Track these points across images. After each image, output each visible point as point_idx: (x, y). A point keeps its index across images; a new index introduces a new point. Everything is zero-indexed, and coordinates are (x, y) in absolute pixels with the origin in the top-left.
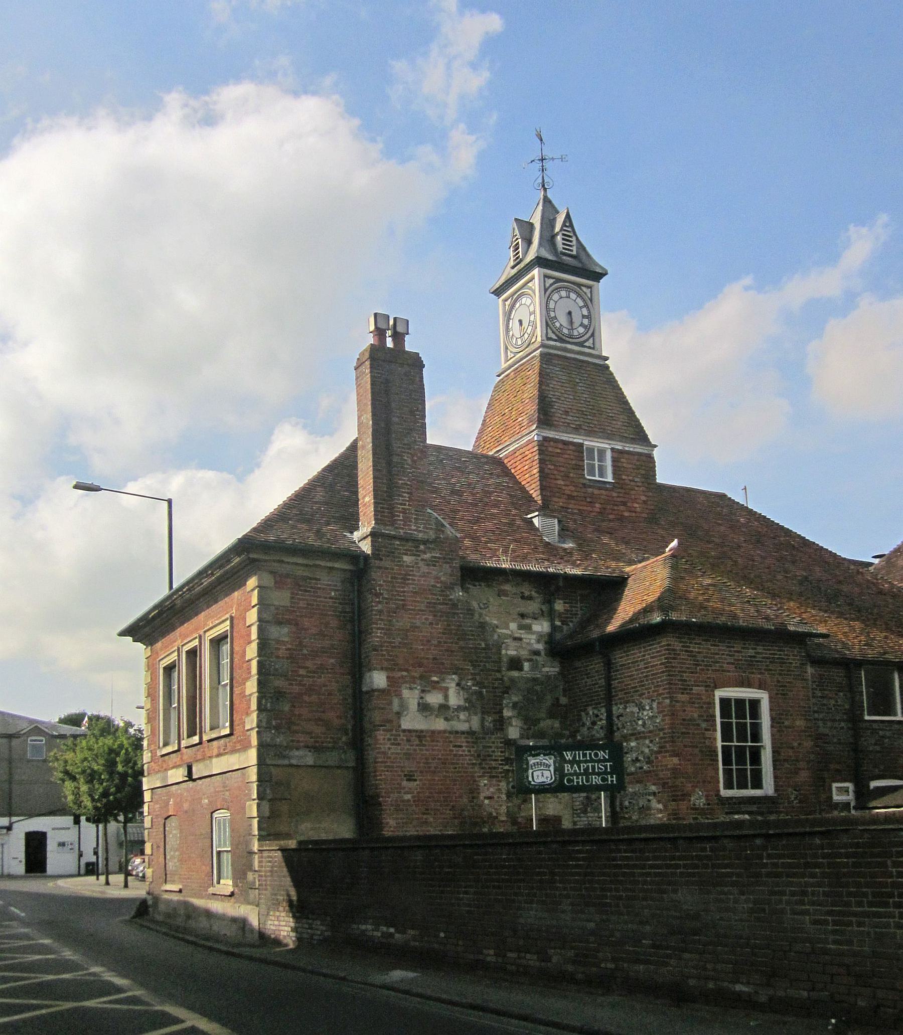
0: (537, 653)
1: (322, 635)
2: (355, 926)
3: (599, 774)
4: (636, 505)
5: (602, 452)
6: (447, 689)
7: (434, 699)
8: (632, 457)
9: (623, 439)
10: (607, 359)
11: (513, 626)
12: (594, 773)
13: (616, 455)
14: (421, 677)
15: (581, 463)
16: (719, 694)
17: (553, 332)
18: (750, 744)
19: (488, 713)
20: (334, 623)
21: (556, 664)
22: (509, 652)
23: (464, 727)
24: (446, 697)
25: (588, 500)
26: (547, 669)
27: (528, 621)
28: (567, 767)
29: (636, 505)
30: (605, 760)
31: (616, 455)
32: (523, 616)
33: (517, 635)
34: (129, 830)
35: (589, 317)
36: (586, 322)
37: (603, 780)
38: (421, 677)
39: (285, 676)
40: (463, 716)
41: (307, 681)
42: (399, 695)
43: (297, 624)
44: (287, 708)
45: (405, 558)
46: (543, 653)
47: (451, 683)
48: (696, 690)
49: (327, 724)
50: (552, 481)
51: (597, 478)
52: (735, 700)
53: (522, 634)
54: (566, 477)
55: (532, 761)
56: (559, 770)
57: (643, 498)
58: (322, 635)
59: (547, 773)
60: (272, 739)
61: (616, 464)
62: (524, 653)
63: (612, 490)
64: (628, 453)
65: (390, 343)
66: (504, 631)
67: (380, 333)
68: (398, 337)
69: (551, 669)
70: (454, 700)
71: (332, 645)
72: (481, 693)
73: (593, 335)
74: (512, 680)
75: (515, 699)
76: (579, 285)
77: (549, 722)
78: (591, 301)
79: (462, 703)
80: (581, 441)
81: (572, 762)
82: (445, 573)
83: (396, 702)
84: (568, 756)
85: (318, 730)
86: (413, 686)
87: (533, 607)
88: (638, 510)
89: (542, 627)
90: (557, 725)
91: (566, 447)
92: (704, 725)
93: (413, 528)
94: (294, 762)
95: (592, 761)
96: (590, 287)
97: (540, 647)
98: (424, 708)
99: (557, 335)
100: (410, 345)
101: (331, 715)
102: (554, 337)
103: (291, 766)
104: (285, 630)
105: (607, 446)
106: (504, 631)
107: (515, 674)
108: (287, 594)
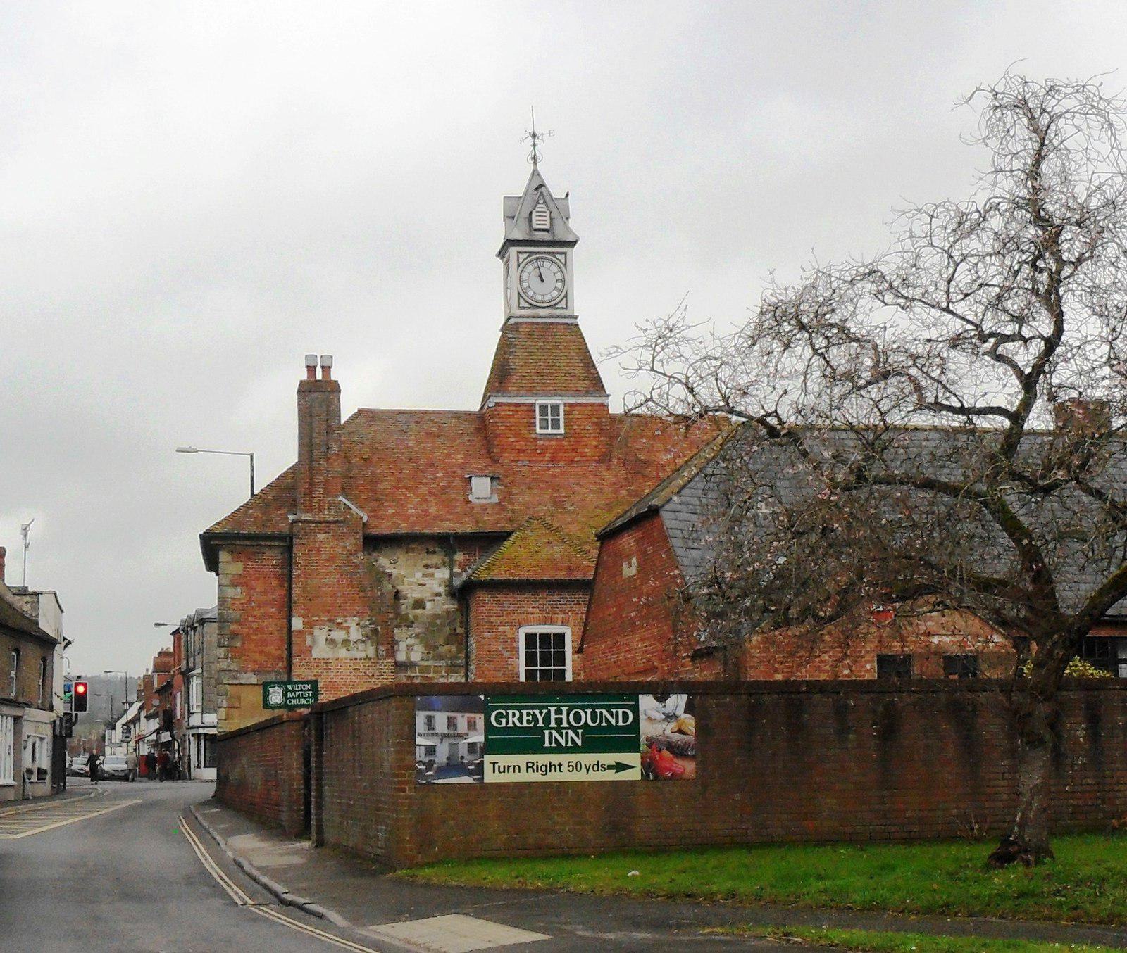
0: (438, 595)
1: (265, 592)
2: (259, 788)
3: (305, 698)
4: (587, 450)
5: (555, 409)
6: (349, 628)
7: (339, 635)
8: (584, 408)
9: (578, 393)
10: (576, 317)
11: (419, 575)
12: (303, 697)
13: (567, 408)
14: (329, 620)
15: (532, 421)
16: (523, 632)
17: (526, 301)
18: (539, 667)
19: (382, 644)
20: (275, 582)
21: (456, 602)
22: (414, 596)
23: (363, 655)
24: (348, 633)
25: (538, 451)
26: (446, 607)
27: (430, 571)
28: (289, 694)
29: (587, 450)
30: (309, 690)
31: (567, 408)
32: (427, 567)
33: (421, 582)
34: (44, 726)
35: (563, 281)
36: (560, 285)
37: (308, 701)
38: (329, 620)
39: (238, 622)
40: (361, 646)
41: (255, 626)
42: (312, 634)
43: (247, 586)
44: (238, 644)
45: (319, 535)
46: (443, 594)
47: (352, 623)
48: (501, 629)
49: (268, 654)
50: (505, 440)
51: (550, 431)
52: (540, 635)
53: (426, 580)
54: (517, 434)
55: (271, 690)
56: (285, 695)
57: (595, 443)
58: (265, 592)
59: (279, 697)
60: (228, 666)
61: (567, 416)
62: (427, 595)
63: (563, 440)
64: (580, 405)
65: (319, 376)
66: (411, 580)
67: (311, 369)
68: (326, 369)
69: (452, 607)
70: (355, 634)
71: (273, 599)
72: (376, 629)
73: (566, 296)
74: (416, 617)
75: (418, 631)
76: (553, 254)
77: (447, 647)
78: (519, 293)
79: (361, 637)
80: (534, 402)
81: (292, 691)
82: (351, 543)
83: (309, 638)
84: (290, 687)
85: (262, 659)
86: (323, 627)
87: (435, 559)
88: (589, 454)
89: (444, 574)
90: (453, 649)
91: (518, 409)
92: (507, 655)
93: (326, 513)
94: (243, 682)
95: (302, 690)
96: (565, 253)
97: (442, 590)
98: (331, 642)
99: (528, 303)
100: (334, 376)
101: (271, 648)
102: (527, 305)
103: (241, 684)
104: (239, 590)
105: (558, 402)
106: (411, 580)
107: (419, 611)
108: (240, 565)
